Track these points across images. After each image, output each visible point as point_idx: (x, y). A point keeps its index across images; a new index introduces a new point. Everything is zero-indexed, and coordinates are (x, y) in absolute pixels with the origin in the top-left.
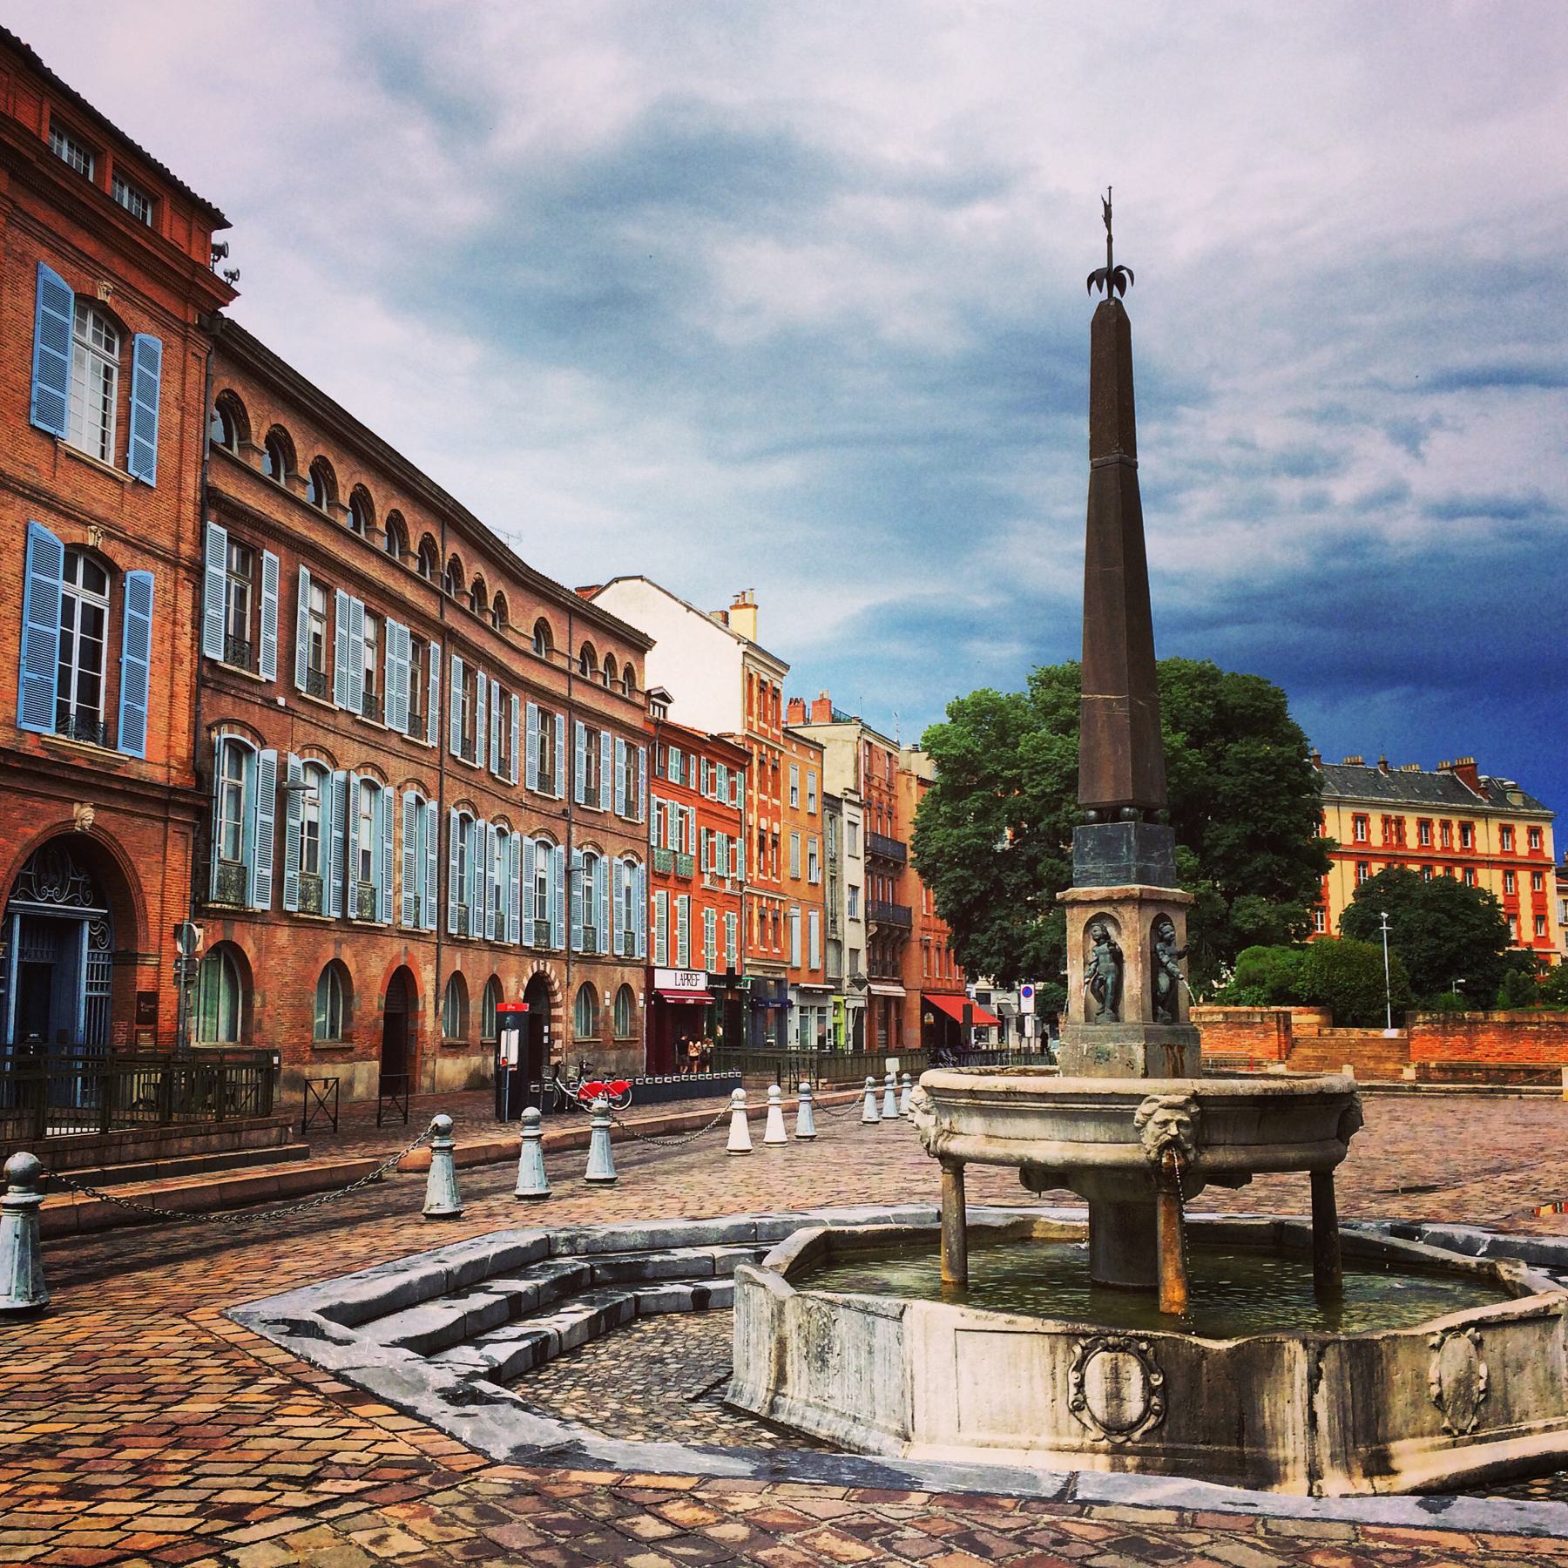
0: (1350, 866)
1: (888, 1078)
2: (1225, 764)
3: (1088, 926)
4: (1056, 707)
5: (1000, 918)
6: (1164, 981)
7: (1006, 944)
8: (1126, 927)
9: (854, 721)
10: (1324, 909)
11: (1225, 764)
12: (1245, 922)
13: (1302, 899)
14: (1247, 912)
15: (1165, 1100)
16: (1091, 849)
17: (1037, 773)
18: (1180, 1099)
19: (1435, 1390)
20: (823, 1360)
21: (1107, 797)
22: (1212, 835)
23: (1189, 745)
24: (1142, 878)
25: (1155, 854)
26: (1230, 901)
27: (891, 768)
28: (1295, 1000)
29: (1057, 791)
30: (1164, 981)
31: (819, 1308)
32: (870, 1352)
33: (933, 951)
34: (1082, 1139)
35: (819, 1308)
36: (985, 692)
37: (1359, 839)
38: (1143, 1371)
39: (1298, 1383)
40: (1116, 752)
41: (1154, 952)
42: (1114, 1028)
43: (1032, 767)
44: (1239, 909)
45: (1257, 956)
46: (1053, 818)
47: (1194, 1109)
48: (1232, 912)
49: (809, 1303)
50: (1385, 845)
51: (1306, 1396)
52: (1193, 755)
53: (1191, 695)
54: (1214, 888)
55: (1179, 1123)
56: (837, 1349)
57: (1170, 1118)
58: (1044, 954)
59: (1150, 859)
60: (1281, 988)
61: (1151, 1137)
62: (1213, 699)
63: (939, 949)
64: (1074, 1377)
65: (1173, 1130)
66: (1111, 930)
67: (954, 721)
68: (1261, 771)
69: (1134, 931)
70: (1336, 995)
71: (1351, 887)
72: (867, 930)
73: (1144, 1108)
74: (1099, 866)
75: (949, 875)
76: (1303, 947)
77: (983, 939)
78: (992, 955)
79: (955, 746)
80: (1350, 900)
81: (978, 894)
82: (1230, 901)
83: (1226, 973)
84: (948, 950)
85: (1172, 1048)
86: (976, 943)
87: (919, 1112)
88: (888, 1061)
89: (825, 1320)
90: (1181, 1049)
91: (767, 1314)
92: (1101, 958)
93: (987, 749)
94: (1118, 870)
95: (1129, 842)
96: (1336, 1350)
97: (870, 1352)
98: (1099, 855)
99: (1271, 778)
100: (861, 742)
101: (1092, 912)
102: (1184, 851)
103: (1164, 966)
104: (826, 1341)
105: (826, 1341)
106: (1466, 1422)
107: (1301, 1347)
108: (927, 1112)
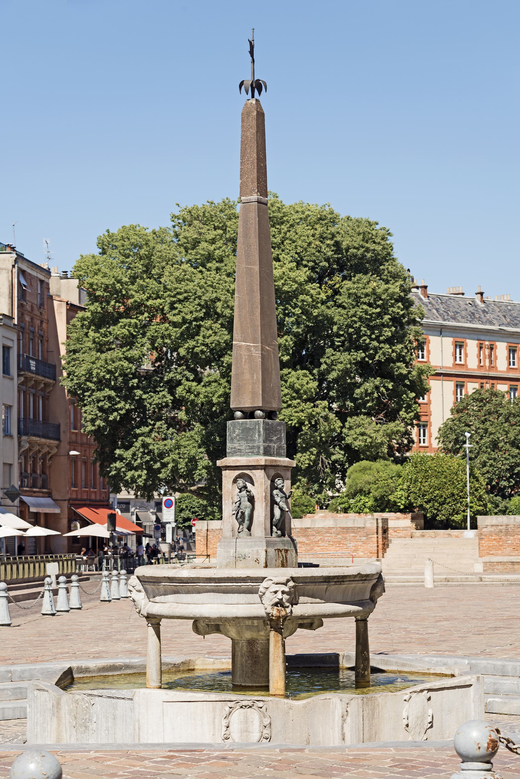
0: (450, 385)
1: (47, 580)
2: (341, 299)
3: (235, 481)
4: (196, 243)
5: (142, 434)
6: (277, 513)
7: (148, 458)
8: (257, 481)
9: (8, 250)
10: (424, 426)
11: (341, 299)
12: (355, 439)
13: (404, 419)
14: (358, 431)
15: (276, 580)
16: (238, 435)
17: (180, 301)
18: (283, 580)
19: (405, 722)
20: (86, 727)
21: (247, 403)
22: (329, 361)
23: (310, 280)
24: (267, 452)
25: (275, 438)
26: (343, 421)
27: (42, 294)
28: (393, 507)
29: (196, 319)
30: (277, 513)
31: (83, 699)
32: (114, 719)
33: (79, 463)
34: (230, 602)
35: (83, 699)
36: (133, 228)
37: (458, 362)
38: (260, 718)
39: (337, 719)
40: (253, 377)
41: (272, 496)
42: (249, 540)
43: (174, 296)
44: (350, 428)
45: (364, 470)
46: (191, 343)
47: (291, 584)
48: (345, 430)
49: (78, 697)
50: (480, 367)
51: (340, 725)
52: (313, 288)
53: (313, 236)
54: (330, 409)
55: (283, 592)
56: (95, 719)
57: (277, 589)
58: (182, 466)
59: (271, 441)
60: (382, 497)
61: (270, 599)
62: (332, 239)
63: (85, 463)
64: (224, 723)
65: (279, 595)
66: (249, 485)
67: (104, 253)
68: (370, 305)
69: (261, 483)
70: (428, 502)
71: (450, 403)
72: (20, 446)
73: (265, 584)
74: (244, 445)
75: (98, 394)
76: (402, 461)
77: (128, 454)
78: (136, 469)
79: (105, 275)
80: (448, 415)
81: (123, 412)
82: (343, 421)
83: (339, 483)
84: (94, 463)
85: (281, 551)
86: (121, 458)
87: (134, 591)
88: (48, 565)
89: (87, 705)
90: (286, 551)
91: (50, 706)
92: (242, 499)
93: (133, 279)
94: (253, 447)
95: (259, 432)
96: (356, 701)
97: (114, 719)
98: (242, 439)
99: (378, 310)
100: (15, 270)
101: (237, 472)
102: (305, 375)
103: (277, 504)
104: (88, 716)
105: (88, 716)
106: (421, 738)
107: (339, 701)
108: (139, 591)
